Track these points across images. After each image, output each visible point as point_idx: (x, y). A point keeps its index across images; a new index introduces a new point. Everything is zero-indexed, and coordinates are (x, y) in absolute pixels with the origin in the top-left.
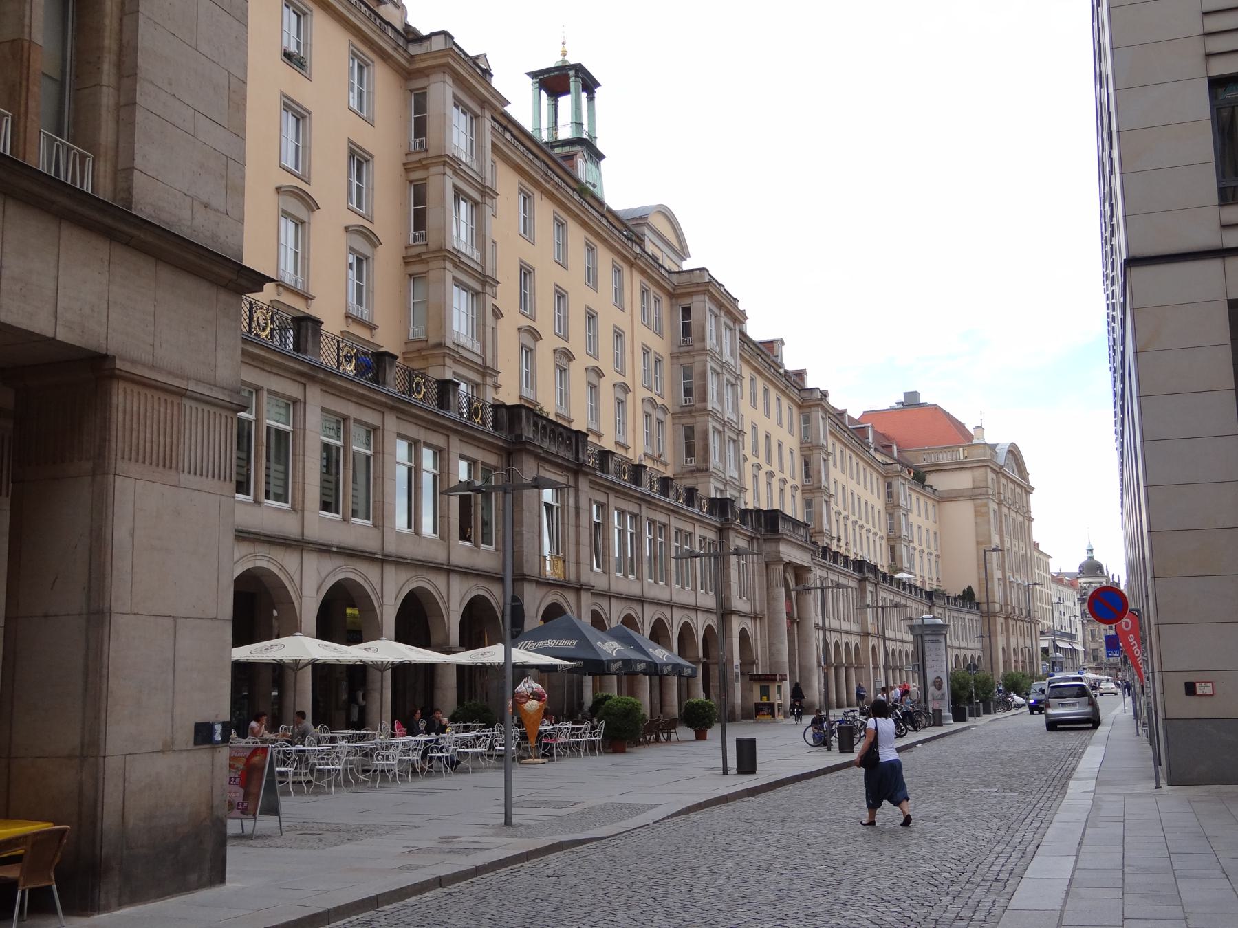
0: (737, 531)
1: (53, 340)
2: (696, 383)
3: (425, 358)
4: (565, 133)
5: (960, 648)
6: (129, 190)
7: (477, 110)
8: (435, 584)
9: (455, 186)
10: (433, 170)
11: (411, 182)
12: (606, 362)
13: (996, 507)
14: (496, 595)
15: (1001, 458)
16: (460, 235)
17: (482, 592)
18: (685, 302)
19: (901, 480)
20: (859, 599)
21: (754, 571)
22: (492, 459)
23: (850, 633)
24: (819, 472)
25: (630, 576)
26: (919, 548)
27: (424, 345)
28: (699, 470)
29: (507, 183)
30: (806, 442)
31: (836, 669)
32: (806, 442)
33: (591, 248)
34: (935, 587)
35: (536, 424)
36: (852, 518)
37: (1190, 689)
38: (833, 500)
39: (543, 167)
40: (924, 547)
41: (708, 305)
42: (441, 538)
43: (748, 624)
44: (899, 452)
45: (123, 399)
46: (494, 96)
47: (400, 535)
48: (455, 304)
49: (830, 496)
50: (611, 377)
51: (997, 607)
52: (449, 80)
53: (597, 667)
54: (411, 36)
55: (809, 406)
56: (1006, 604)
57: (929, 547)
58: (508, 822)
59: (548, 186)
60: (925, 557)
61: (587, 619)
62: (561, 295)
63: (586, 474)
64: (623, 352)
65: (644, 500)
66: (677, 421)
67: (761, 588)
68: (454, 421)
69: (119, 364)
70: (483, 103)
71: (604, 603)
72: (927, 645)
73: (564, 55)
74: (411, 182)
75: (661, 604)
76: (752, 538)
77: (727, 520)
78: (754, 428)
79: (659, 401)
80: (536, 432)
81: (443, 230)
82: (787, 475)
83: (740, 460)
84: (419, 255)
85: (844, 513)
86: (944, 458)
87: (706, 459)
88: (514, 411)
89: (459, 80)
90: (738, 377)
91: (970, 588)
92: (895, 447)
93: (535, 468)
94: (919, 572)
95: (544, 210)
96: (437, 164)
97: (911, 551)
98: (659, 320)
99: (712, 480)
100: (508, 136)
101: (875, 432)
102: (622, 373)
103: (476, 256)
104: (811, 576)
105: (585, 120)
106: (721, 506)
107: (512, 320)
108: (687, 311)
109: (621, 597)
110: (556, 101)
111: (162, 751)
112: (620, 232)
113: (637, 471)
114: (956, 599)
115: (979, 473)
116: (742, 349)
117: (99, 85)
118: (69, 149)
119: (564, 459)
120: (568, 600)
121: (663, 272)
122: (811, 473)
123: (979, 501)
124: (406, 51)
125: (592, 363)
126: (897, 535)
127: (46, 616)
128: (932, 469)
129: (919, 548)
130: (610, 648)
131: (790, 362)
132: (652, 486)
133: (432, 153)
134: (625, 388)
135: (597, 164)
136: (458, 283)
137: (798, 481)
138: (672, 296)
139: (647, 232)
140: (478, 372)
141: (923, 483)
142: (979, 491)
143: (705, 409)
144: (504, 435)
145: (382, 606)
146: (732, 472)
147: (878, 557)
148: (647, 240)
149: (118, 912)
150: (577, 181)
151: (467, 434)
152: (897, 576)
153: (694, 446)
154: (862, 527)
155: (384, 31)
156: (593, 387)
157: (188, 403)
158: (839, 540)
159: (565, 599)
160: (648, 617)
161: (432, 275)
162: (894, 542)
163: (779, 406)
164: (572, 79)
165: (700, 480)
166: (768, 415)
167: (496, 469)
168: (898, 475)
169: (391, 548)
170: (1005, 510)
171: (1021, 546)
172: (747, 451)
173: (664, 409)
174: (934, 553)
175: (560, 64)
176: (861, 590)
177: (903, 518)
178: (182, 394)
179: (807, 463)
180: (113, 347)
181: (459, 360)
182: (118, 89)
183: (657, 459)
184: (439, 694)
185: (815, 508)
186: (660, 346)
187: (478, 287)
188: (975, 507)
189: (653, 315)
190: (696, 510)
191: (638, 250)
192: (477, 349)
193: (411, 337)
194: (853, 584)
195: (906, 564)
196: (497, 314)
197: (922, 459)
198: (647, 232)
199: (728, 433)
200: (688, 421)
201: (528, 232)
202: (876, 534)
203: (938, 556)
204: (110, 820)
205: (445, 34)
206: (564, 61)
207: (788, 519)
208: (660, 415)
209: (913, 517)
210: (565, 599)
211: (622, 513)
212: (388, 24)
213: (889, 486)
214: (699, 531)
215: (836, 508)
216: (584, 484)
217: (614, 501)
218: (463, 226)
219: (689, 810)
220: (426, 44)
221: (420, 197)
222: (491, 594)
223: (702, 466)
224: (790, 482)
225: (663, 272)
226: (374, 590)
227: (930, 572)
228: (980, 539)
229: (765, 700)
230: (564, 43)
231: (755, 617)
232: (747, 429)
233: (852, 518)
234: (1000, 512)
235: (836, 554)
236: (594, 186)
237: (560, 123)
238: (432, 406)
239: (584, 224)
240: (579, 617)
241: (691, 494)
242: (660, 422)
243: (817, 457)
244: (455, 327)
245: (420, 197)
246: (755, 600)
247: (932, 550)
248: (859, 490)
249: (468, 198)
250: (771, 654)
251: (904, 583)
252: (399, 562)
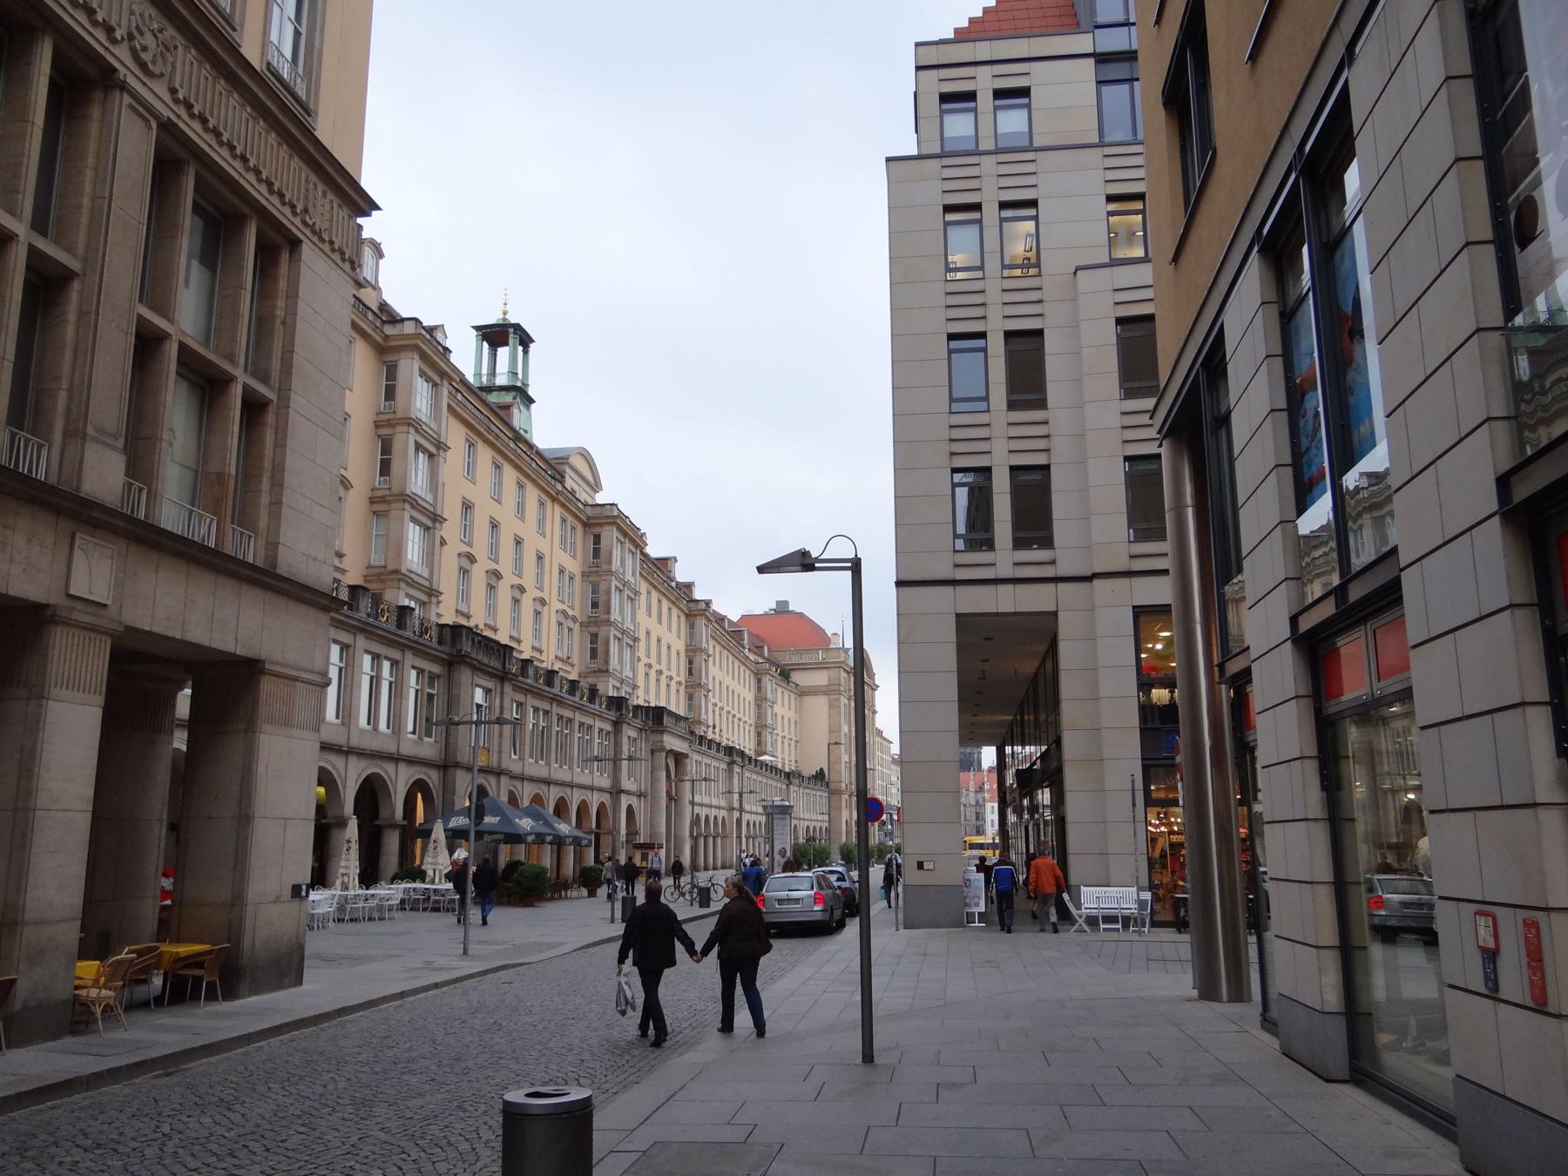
0: (629, 724)
1: (234, 654)
2: (602, 599)
3: (383, 581)
4: (501, 380)
5: (811, 820)
6: (275, 556)
7: (438, 380)
8: (386, 770)
9: (416, 442)
10: (398, 429)
11: (379, 436)
12: (528, 580)
13: (846, 701)
14: (433, 778)
16: (417, 482)
17: (422, 776)
18: (597, 530)
19: (768, 677)
22: (436, 669)
23: (718, 808)
24: (701, 671)
25: (541, 762)
26: (781, 734)
27: (383, 570)
28: (600, 671)
29: (455, 435)
30: (691, 645)
31: (705, 838)
32: (691, 645)
33: (521, 486)
34: (793, 768)
35: (473, 640)
36: (726, 709)
37: (920, 865)
38: (711, 694)
39: (486, 421)
40: (786, 734)
41: (616, 534)
42: (393, 732)
43: (634, 801)
44: (769, 651)
45: (267, 686)
46: (452, 370)
47: (362, 731)
48: (410, 537)
49: (709, 691)
50: (532, 593)
51: (843, 785)
52: (416, 357)
53: (514, 838)
54: (387, 315)
55: (695, 615)
58: (465, 952)
59: (490, 437)
60: (786, 741)
61: (504, 798)
62: (494, 525)
63: (510, 680)
64: (543, 572)
65: (555, 700)
66: (584, 629)
67: (646, 771)
68: (409, 640)
69: (267, 666)
70: (443, 374)
71: (518, 784)
72: (775, 822)
73: (505, 313)
74: (379, 436)
75: (564, 784)
76: (641, 730)
77: (622, 715)
78: (648, 633)
79: (570, 612)
80: (473, 646)
81: (404, 478)
82: (673, 673)
83: (635, 660)
84: (383, 497)
85: (720, 705)
86: (806, 659)
87: (607, 662)
88: (456, 629)
89: (424, 357)
90: (637, 593)
91: (822, 769)
92: (766, 648)
93: (470, 676)
94: (781, 755)
95: (485, 455)
96: (403, 424)
97: (775, 737)
98: (574, 544)
99: (611, 679)
100: (459, 396)
101: (749, 633)
102: (541, 589)
103: (429, 498)
104: (688, 761)
105: (520, 371)
106: (618, 703)
107: (455, 546)
108: (597, 539)
109: (532, 780)
110: (496, 351)
111: (275, 902)
112: (546, 472)
113: (551, 675)
114: (809, 778)
115: (833, 672)
116: (642, 568)
117: (260, 491)
118: (242, 533)
119: (493, 668)
120: (490, 783)
121: (580, 505)
122: (694, 671)
123: (832, 697)
124: (382, 331)
125: (517, 581)
127: (210, 818)
129: (781, 734)
130: (526, 824)
131: (681, 574)
132: (562, 688)
133: (399, 415)
134: (543, 602)
135: (528, 408)
136: (414, 520)
137: (682, 679)
138: (586, 525)
139: (568, 470)
140: (425, 593)
142: (832, 688)
143: (608, 621)
144: (447, 649)
145: (344, 788)
146: (628, 673)
147: (747, 744)
148: (567, 477)
149: (254, 999)
150: (512, 429)
151: (420, 651)
152: (761, 758)
153: (597, 650)
154: (734, 716)
155: (365, 316)
156: (516, 601)
157: (298, 684)
158: (714, 727)
159: (488, 781)
160: (553, 795)
161: (393, 514)
162: (760, 729)
164: (511, 335)
165: (601, 679)
166: (660, 622)
167: (439, 676)
168: (767, 672)
169: (355, 741)
172: (641, 653)
173: (574, 619)
174: (794, 739)
175: (501, 322)
176: (730, 771)
177: (769, 710)
178: (296, 679)
179: (691, 663)
180: (263, 655)
181: (412, 584)
182: (271, 494)
183: (566, 661)
184: (384, 859)
185: (695, 701)
186: (574, 566)
187: (429, 523)
189: (569, 541)
190: (597, 707)
191: (559, 487)
192: (426, 574)
193: (372, 563)
194: (724, 766)
195: (769, 748)
196: (443, 543)
197: (787, 659)
198: (568, 470)
199: (626, 640)
200: (593, 629)
201: (470, 468)
202: (745, 722)
203: (797, 742)
204: (247, 942)
205: (416, 320)
206: (505, 319)
207: (671, 714)
208: (570, 623)
209: (777, 708)
210: (488, 781)
211: (536, 710)
212: (369, 309)
213: (759, 681)
214: (598, 724)
215: (713, 701)
216: (508, 688)
217: (531, 701)
218: (420, 473)
219: (588, 946)
220: (399, 326)
221: (387, 448)
222: (430, 777)
223: (603, 667)
224: (676, 678)
225: (580, 505)
226: (340, 776)
227: (790, 755)
228: (832, 728)
230: (505, 304)
231: (640, 795)
232: (642, 636)
233: (726, 709)
235: (710, 741)
236: (526, 432)
237: (497, 371)
238: (392, 627)
239: (517, 467)
240: (499, 796)
241: (593, 693)
242: (570, 630)
243: (699, 659)
244: (409, 557)
245: (387, 448)
247: (793, 736)
248: (733, 685)
249: (425, 451)
250: (652, 826)
251: (767, 765)
252: (361, 753)
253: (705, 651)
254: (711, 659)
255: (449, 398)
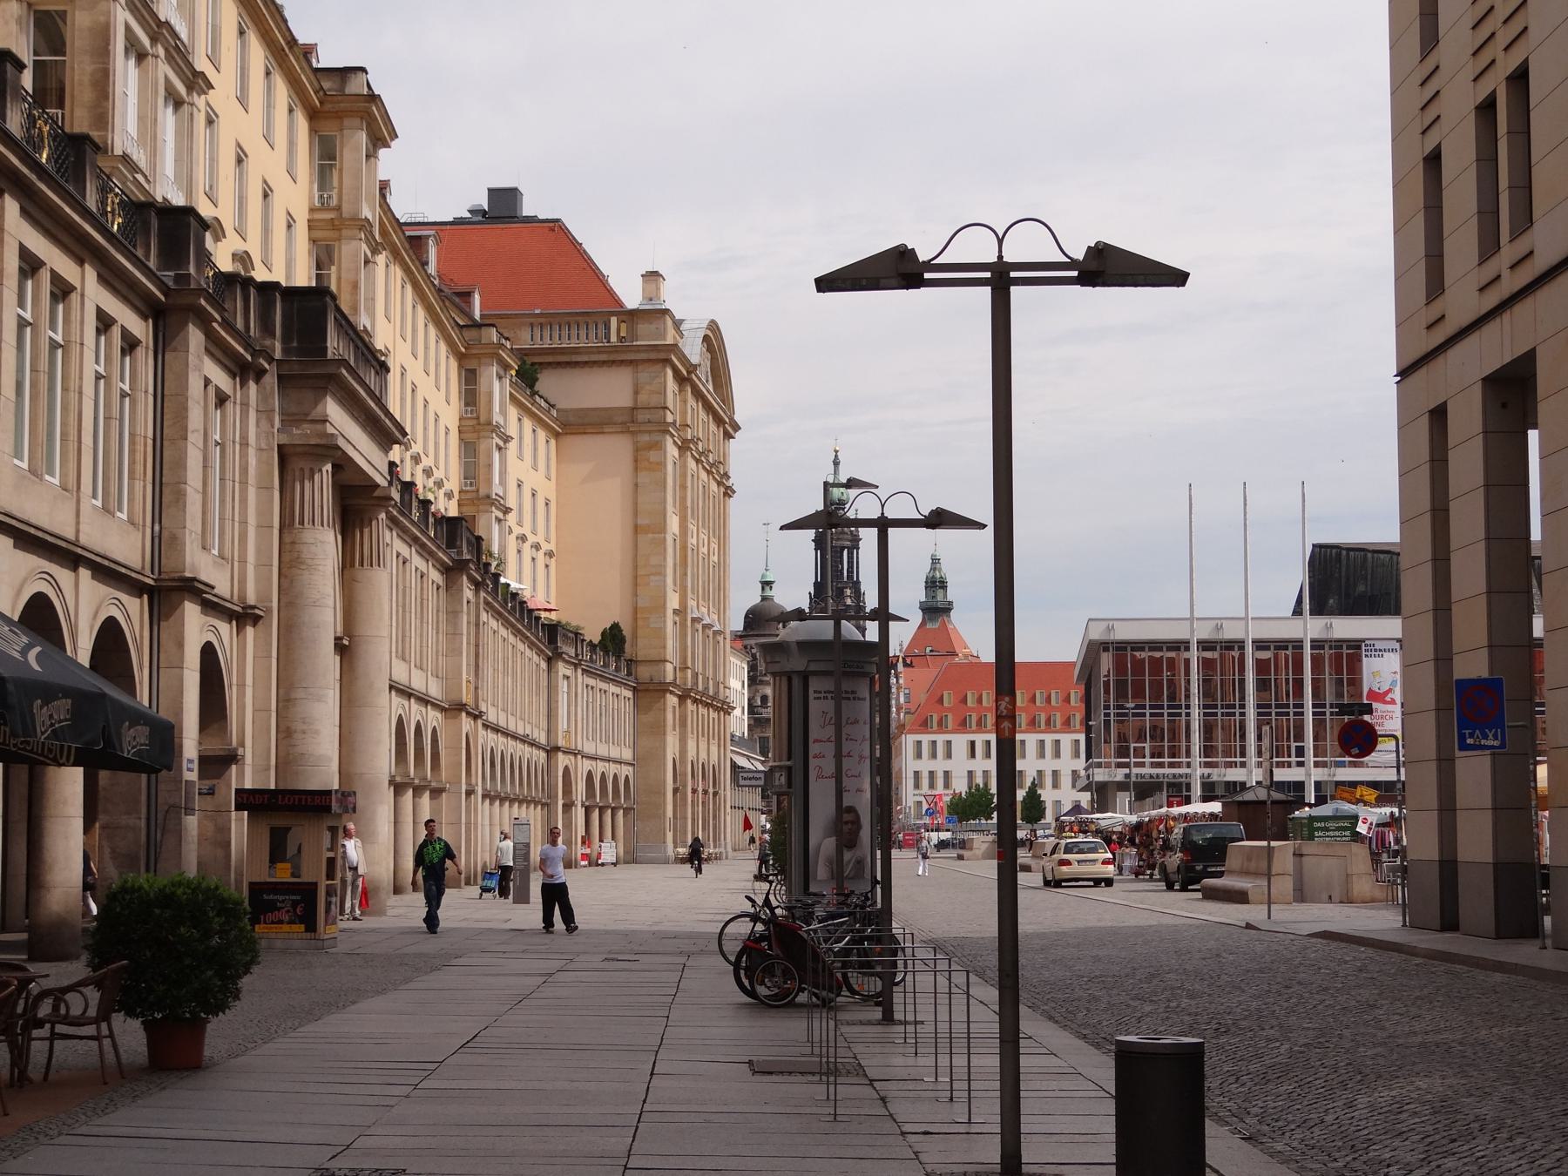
15: (694, 351)
20: (443, 617)
21: (244, 470)
26: (517, 531)
32: (324, 207)
56: (684, 668)
57: (534, 532)
67: (264, 527)
123: (645, 438)
126: (482, 492)
128: (550, 359)
141: (531, 386)
154: (523, 538)
163: (269, 90)
170: (692, 464)
171: (712, 545)
188: (637, 450)
202: (537, 547)
229: (283, 874)
234: (684, 466)
246: (243, 561)
250: (286, 733)
253: (495, 429)
254: (513, 446)
255: (510, 386)
